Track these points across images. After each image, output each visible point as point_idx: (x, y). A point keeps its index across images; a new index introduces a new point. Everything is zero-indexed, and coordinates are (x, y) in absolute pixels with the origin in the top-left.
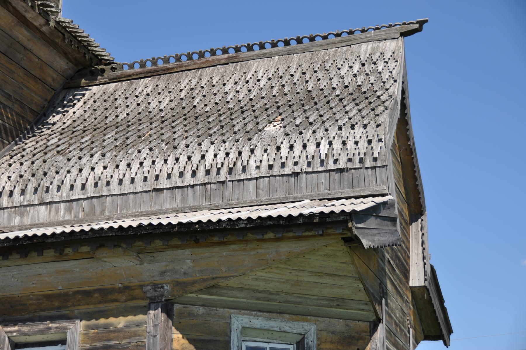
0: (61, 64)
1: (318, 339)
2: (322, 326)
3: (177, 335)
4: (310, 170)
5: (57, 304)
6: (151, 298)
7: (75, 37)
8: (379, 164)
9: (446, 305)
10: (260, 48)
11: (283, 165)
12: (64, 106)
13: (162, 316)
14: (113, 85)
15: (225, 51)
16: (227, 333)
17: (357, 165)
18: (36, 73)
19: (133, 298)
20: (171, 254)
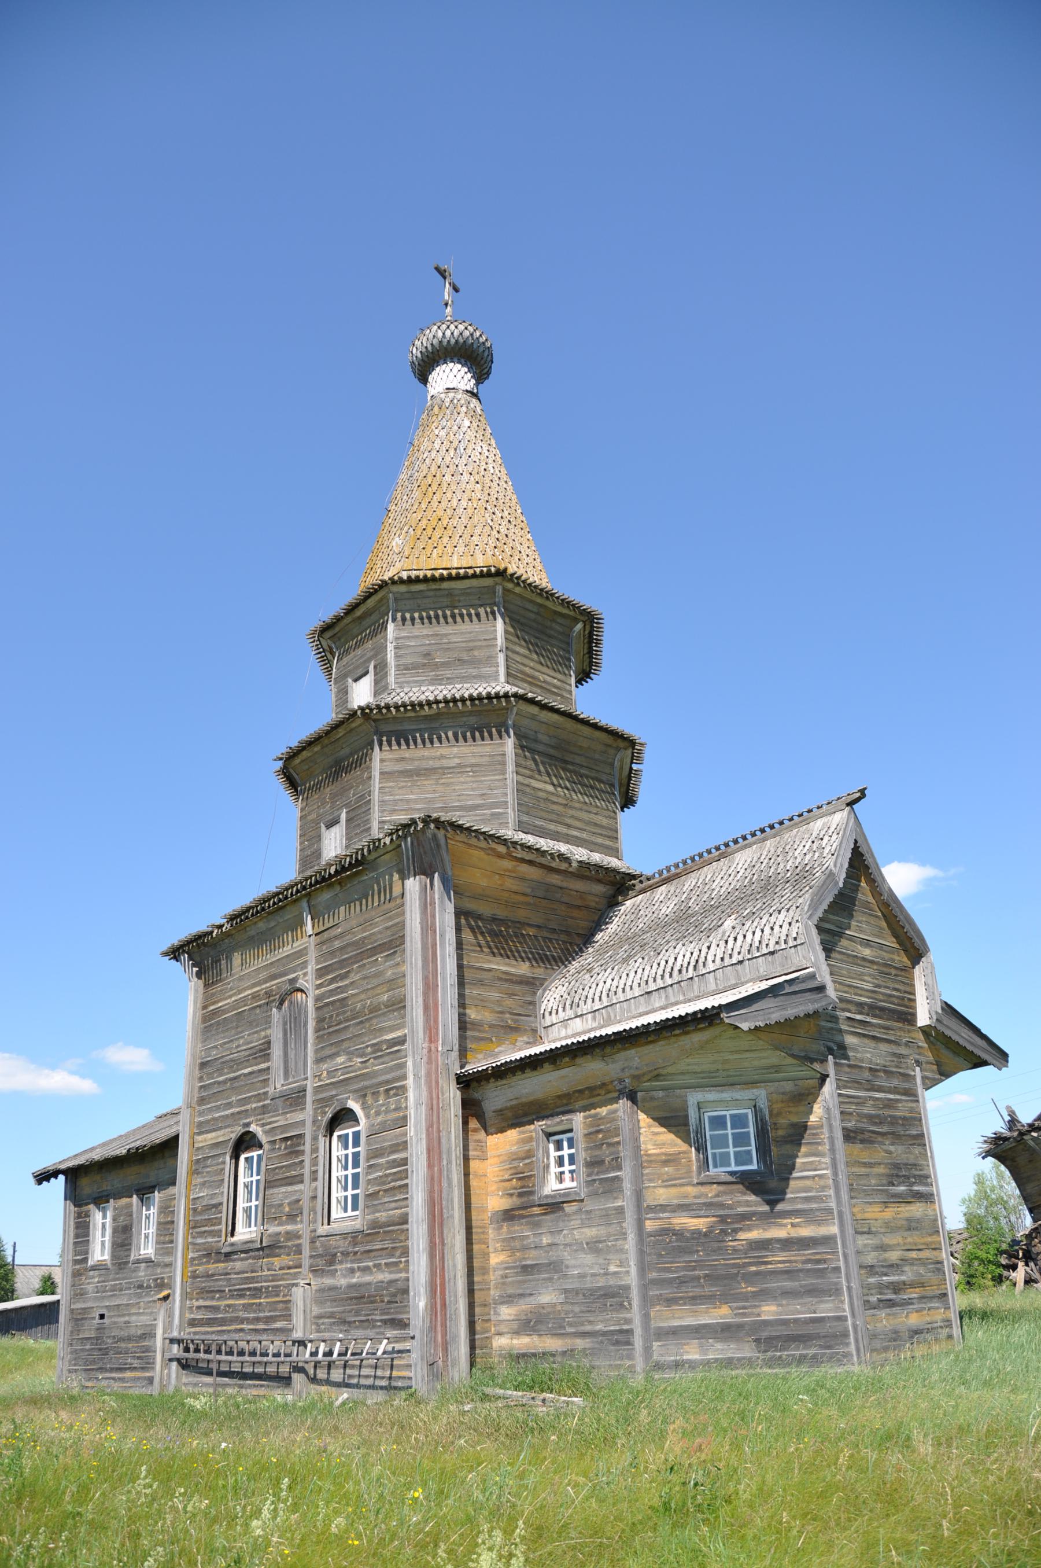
0: (599, 889)
1: (769, 1101)
2: (772, 1089)
3: (642, 1116)
4: (750, 957)
5: (565, 1101)
6: (619, 1091)
7: (601, 867)
8: (799, 942)
9: (984, 1031)
10: (741, 841)
11: (731, 956)
12: (607, 923)
13: (629, 1103)
14: (640, 897)
15: (718, 848)
16: (686, 1109)
17: (783, 946)
18: (579, 903)
19: (609, 1092)
20: (623, 1055)
